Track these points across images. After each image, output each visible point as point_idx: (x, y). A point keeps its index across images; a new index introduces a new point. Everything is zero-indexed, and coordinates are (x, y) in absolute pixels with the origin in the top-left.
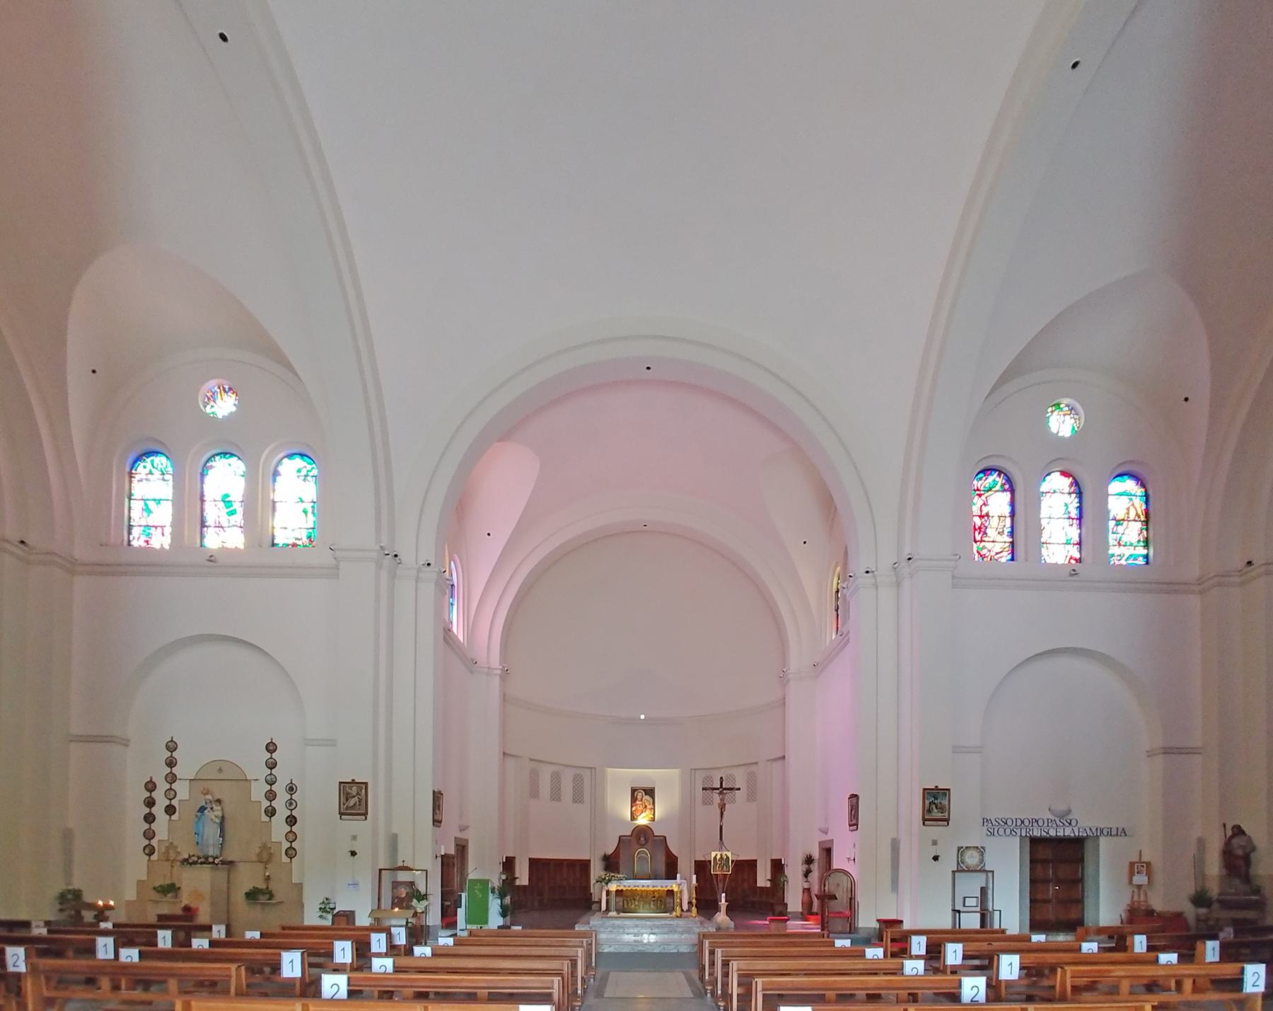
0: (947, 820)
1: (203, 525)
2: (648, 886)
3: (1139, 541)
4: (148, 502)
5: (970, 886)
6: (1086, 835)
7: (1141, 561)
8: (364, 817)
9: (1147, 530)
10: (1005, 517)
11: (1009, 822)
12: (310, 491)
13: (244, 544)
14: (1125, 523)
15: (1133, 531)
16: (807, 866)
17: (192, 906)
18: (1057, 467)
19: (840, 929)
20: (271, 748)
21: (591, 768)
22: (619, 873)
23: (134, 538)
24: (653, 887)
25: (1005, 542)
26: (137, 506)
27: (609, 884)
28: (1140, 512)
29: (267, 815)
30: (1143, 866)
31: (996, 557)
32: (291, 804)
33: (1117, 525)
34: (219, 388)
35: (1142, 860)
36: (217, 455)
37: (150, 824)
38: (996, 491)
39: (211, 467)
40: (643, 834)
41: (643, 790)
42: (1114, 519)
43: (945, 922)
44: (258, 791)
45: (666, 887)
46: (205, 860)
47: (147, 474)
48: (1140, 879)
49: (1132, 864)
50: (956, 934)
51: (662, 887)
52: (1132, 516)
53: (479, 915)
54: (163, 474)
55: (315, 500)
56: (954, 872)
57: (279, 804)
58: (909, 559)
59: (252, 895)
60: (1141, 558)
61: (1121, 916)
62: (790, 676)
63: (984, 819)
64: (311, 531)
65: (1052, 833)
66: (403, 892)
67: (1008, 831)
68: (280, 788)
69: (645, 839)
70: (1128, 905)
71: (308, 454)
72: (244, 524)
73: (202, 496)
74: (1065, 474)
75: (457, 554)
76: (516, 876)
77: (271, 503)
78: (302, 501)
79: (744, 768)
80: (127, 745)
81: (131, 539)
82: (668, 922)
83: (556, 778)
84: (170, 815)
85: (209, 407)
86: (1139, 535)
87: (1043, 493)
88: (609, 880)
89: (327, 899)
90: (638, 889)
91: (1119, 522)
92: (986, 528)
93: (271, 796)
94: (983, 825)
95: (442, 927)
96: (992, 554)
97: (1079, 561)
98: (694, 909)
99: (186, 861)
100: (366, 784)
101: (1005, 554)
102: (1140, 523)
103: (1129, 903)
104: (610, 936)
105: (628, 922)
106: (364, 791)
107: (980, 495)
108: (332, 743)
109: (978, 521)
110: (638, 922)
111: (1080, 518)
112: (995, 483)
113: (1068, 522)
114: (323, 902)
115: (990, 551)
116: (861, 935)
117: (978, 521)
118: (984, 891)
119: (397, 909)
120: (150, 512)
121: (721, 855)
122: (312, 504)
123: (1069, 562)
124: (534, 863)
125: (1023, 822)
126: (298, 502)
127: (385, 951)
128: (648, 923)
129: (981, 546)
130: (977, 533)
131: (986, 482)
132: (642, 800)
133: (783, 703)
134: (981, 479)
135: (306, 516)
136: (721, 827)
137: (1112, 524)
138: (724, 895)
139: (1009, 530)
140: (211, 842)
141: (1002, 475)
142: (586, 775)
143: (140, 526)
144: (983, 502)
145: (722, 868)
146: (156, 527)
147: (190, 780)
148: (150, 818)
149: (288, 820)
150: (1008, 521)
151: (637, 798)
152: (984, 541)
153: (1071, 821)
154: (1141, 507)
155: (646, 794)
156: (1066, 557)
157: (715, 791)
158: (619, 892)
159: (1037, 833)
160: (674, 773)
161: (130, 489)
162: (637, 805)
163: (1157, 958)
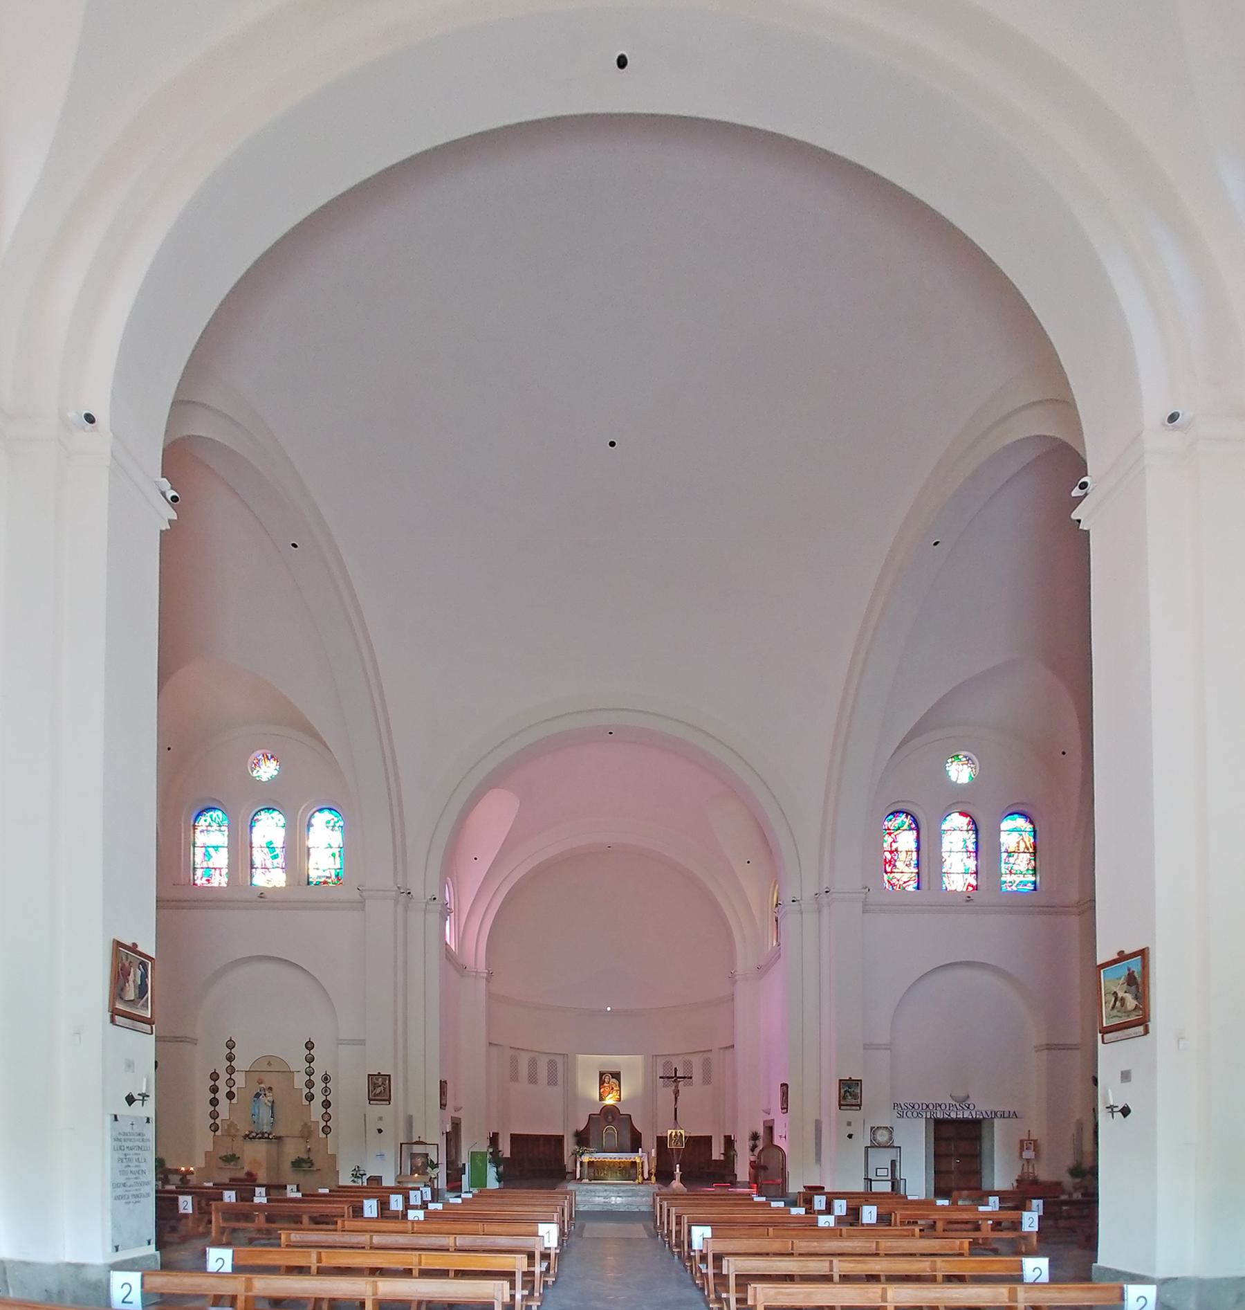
0: (860, 1106)
1: (252, 867)
2: (615, 1158)
3: (1028, 870)
4: (208, 849)
5: (881, 1160)
6: (981, 1117)
7: (1031, 887)
8: (388, 1102)
9: (1035, 860)
10: (912, 851)
11: (916, 1107)
12: (337, 838)
13: (286, 882)
14: (1016, 855)
15: (1023, 862)
16: (753, 1142)
17: (254, 1172)
18: (957, 809)
19: (774, 1194)
20: (309, 1046)
21: (564, 1054)
22: (590, 1148)
23: (198, 878)
24: (619, 1159)
25: (912, 873)
26: (199, 853)
27: (583, 1156)
28: (1029, 846)
29: (307, 1100)
30: (1031, 1143)
31: (904, 885)
32: (326, 1090)
33: (1009, 857)
34: (263, 756)
35: (1031, 1138)
36: (262, 810)
37: (215, 1106)
38: (904, 830)
39: (257, 820)
40: (610, 1113)
41: (610, 1074)
42: (1007, 851)
43: (860, 1187)
44: (300, 1081)
45: (630, 1159)
46: (262, 1136)
47: (207, 826)
48: (1029, 1154)
49: (1022, 1142)
50: (869, 1197)
51: (627, 1159)
52: (1022, 848)
53: (479, 1180)
54: (220, 826)
55: (341, 846)
56: (867, 1148)
57: (317, 1090)
58: (827, 892)
59: (297, 1164)
60: (1030, 885)
61: (1013, 1184)
62: (737, 977)
63: (894, 1104)
64: (338, 871)
65: (953, 1115)
66: (419, 1161)
67: (915, 1114)
68: (317, 1078)
69: (613, 1118)
70: (1019, 1176)
71: (334, 808)
72: (286, 865)
73: (251, 843)
74: (963, 814)
75: (450, 878)
76: (500, 1149)
77: (306, 849)
78: (331, 847)
79: (701, 1054)
80: (196, 1044)
81: (196, 878)
82: (632, 1188)
83: (533, 1064)
84: (230, 1100)
85: (255, 771)
86: (1028, 864)
87: (944, 830)
88: (583, 1153)
89: (358, 1167)
90: (607, 1160)
91: (1010, 854)
92: (895, 861)
93: (310, 1084)
94: (894, 1108)
95: (448, 1191)
96: (901, 883)
97: (976, 888)
98: (653, 1178)
99: (246, 1137)
100: (389, 1076)
101: (911, 882)
102: (1028, 854)
103: (1020, 1174)
104: (584, 1199)
105: (598, 1187)
106: (387, 1081)
107: (890, 834)
108: (362, 1042)
109: (888, 856)
110: (606, 1188)
111: (976, 852)
112: (903, 823)
113: (965, 855)
114: (355, 1169)
115: (898, 880)
116: (791, 1198)
117: (888, 856)
118: (893, 1163)
119: (416, 1175)
120: (211, 856)
121: (676, 1132)
122: (339, 849)
123: (967, 889)
124: (514, 1137)
125: (927, 1106)
126: (327, 848)
127: (376, 1216)
128: (615, 1188)
129: (891, 877)
130: (887, 865)
131: (896, 822)
132: (609, 1083)
133: (732, 998)
134: (891, 820)
135: (335, 859)
136: (676, 1109)
137: (1004, 855)
138: (678, 1166)
139: (916, 862)
140: (265, 1121)
141: (909, 816)
142: (559, 1060)
143: (202, 868)
144: (892, 840)
145: (677, 1144)
146: (215, 869)
147: (246, 1071)
148: (214, 1102)
149: (324, 1104)
150: (915, 855)
151: (604, 1081)
152: (894, 872)
153: (969, 1105)
154: (1029, 841)
155: (613, 1078)
156: (965, 884)
157: (670, 1080)
158: (591, 1163)
159: (940, 1116)
160: (638, 1059)
161: (194, 839)
162: (605, 1087)
163: (978, 1208)
